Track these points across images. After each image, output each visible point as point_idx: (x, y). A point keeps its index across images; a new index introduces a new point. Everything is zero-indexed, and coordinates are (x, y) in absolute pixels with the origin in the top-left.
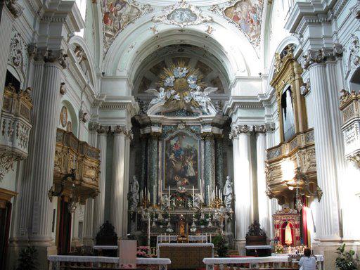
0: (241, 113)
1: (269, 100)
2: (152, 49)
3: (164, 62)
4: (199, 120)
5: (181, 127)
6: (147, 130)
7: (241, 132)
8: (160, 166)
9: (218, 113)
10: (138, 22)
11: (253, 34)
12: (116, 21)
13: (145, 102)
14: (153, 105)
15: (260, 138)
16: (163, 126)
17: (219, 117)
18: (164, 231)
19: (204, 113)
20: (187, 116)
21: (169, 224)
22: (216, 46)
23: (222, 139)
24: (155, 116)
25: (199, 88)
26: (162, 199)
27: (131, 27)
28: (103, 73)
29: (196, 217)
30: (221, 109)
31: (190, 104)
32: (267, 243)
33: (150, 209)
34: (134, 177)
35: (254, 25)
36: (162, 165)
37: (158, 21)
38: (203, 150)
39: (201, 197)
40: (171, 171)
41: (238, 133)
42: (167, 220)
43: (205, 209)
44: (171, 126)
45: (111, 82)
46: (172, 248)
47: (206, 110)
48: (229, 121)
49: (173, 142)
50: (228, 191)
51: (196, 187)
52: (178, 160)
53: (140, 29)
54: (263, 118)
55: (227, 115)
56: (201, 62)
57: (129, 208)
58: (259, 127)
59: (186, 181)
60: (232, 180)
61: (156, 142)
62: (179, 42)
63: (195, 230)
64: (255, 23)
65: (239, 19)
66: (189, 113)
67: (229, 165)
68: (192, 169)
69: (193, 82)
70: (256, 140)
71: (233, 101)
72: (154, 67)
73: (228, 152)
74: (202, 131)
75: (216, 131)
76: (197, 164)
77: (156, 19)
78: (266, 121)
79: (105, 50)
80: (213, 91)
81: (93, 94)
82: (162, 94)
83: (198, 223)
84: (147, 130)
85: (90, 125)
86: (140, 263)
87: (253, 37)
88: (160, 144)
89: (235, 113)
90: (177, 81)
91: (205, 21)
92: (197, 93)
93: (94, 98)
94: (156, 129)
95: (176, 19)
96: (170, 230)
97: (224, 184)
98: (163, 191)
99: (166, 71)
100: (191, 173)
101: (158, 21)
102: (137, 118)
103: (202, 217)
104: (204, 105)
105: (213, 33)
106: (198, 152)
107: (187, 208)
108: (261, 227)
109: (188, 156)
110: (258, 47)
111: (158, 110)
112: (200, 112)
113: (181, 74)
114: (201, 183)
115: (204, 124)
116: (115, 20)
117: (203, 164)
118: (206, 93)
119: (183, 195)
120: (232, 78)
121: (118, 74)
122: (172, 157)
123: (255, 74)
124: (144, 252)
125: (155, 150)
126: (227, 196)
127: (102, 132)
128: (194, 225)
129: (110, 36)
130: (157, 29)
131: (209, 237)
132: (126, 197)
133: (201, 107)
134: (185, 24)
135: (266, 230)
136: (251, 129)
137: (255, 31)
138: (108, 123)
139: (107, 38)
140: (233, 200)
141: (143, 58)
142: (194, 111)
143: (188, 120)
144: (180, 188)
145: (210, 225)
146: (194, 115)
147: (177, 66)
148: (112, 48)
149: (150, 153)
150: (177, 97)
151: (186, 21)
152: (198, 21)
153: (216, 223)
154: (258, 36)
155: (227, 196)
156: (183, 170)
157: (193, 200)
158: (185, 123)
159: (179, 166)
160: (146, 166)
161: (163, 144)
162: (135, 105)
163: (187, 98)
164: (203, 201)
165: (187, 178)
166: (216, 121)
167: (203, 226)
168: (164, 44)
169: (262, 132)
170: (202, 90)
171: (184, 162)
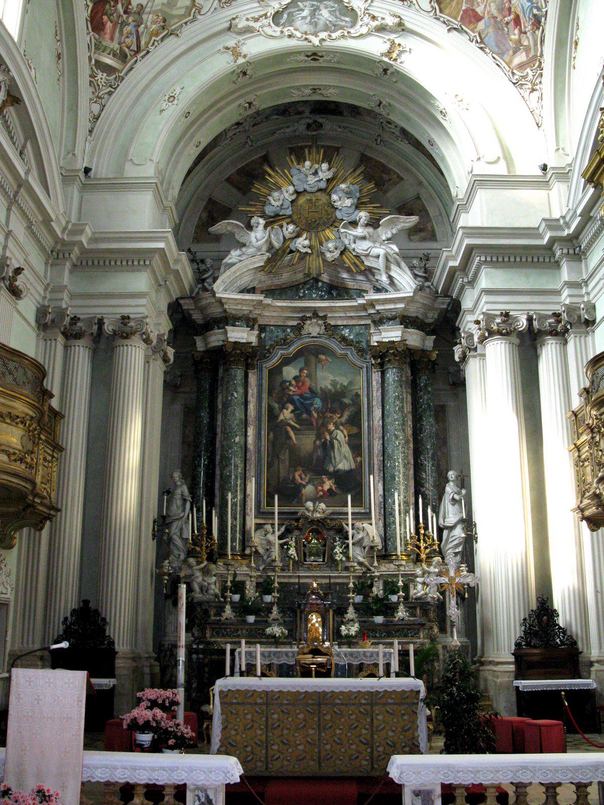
0: (488, 279)
1: (576, 236)
2: (231, 114)
3: (265, 159)
4: (364, 307)
5: (313, 329)
6: (215, 339)
7: (491, 333)
8: (250, 440)
9: (421, 288)
10: (191, 33)
11: (521, 58)
12: (127, 29)
13: (209, 262)
14: (233, 264)
15: (549, 353)
16: (262, 329)
17: (421, 299)
18: (257, 635)
19: (378, 290)
20: (331, 298)
21: (275, 608)
22: (413, 100)
23: (434, 363)
24: (240, 296)
25: (363, 216)
26: (257, 539)
27: (173, 46)
28: (87, 171)
29: (359, 590)
30: (427, 279)
31: (337, 264)
32: (582, 669)
33: (219, 568)
34: (177, 475)
35: (522, 32)
36: (258, 435)
37: (248, 30)
38: (376, 394)
39: (372, 531)
40: (285, 456)
41: (483, 339)
42: (268, 598)
43: (386, 568)
44: (284, 328)
45: (108, 196)
46: (269, 697)
47: (384, 278)
48: (455, 308)
49: (290, 372)
50: (451, 514)
51: (358, 500)
52: (304, 422)
53: (195, 52)
54: (558, 293)
55: (446, 293)
56: (370, 159)
57: (159, 563)
58: (547, 317)
59: (328, 484)
60: (464, 482)
61: (239, 373)
62: (306, 95)
63: (354, 629)
64: (527, 25)
65: (478, 18)
66: (337, 290)
67: (453, 441)
68: (346, 449)
69: (348, 202)
70: (536, 357)
71: (467, 241)
72: (239, 172)
73: (451, 404)
74: (375, 340)
75: (415, 339)
76: (359, 435)
77: (242, 24)
78: (566, 297)
79: (96, 108)
80: (407, 225)
81: (47, 221)
82: (258, 236)
83: (364, 610)
84: (215, 339)
85: (41, 313)
86: (101, 776)
87: (521, 66)
88: (253, 379)
89: (472, 283)
90: (302, 200)
91: (382, 29)
92: (360, 231)
93: (52, 231)
94: (239, 334)
95: (298, 23)
96: (276, 630)
97: (441, 493)
98: (259, 513)
99: (273, 177)
100: (343, 461)
101: (248, 30)
102: (187, 305)
103: (378, 590)
104: (380, 264)
105: (404, 57)
106: (365, 400)
107: (332, 563)
108: (561, 622)
109: (334, 412)
110: (536, 94)
111: (246, 281)
112: (366, 286)
113: (312, 180)
114: (374, 486)
115: (380, 320)
116: (124, 24)
117: (378, 434)
118: (385, 233)
119: (319, 527)
120: (422, 347)
121: (131, 172)
122: (287, 414)
123: (528, 167)
124: (158, 712)
125: (238, 395)
126: (451, 528)
127: (78, 336)
128: (351, 613)
129: (109, 69)
130: (244, 50)
131: (404, 654)
132: (148, 529)
133: (369, 272)
134: (323, 35)
135: (576, 629)
136: (523, 323)
137: (527, 49)
138: (87, 310)
139: (101, 76)
140: (470, 540)
141: (205, 137)
142: (351, 284)
143: (331, 309)
144: (310, 504)
145: (402, 613)
146: (351, 298)
147: (301, 159)
148: (113, 104)
149: (224, 404)
150: (302, 243)
151: (326, 28)
152: (361, 28)
153: (419, 606)
154: (535, 61)
155: (451, 528)
156: (320, 452)
157: (350, 542)
158: (324, 318)
159: (306, 442)
160: (212, 442)
161: (260, 379)
162: (177, 261)
163: (331, 245)
164: (378, 541)
165: (331, 475)
166: (414, 311)
167: (379, 619)
168: (265, 99)
169: (554, 333)
170: (374, 223)
171: (321, 430)
